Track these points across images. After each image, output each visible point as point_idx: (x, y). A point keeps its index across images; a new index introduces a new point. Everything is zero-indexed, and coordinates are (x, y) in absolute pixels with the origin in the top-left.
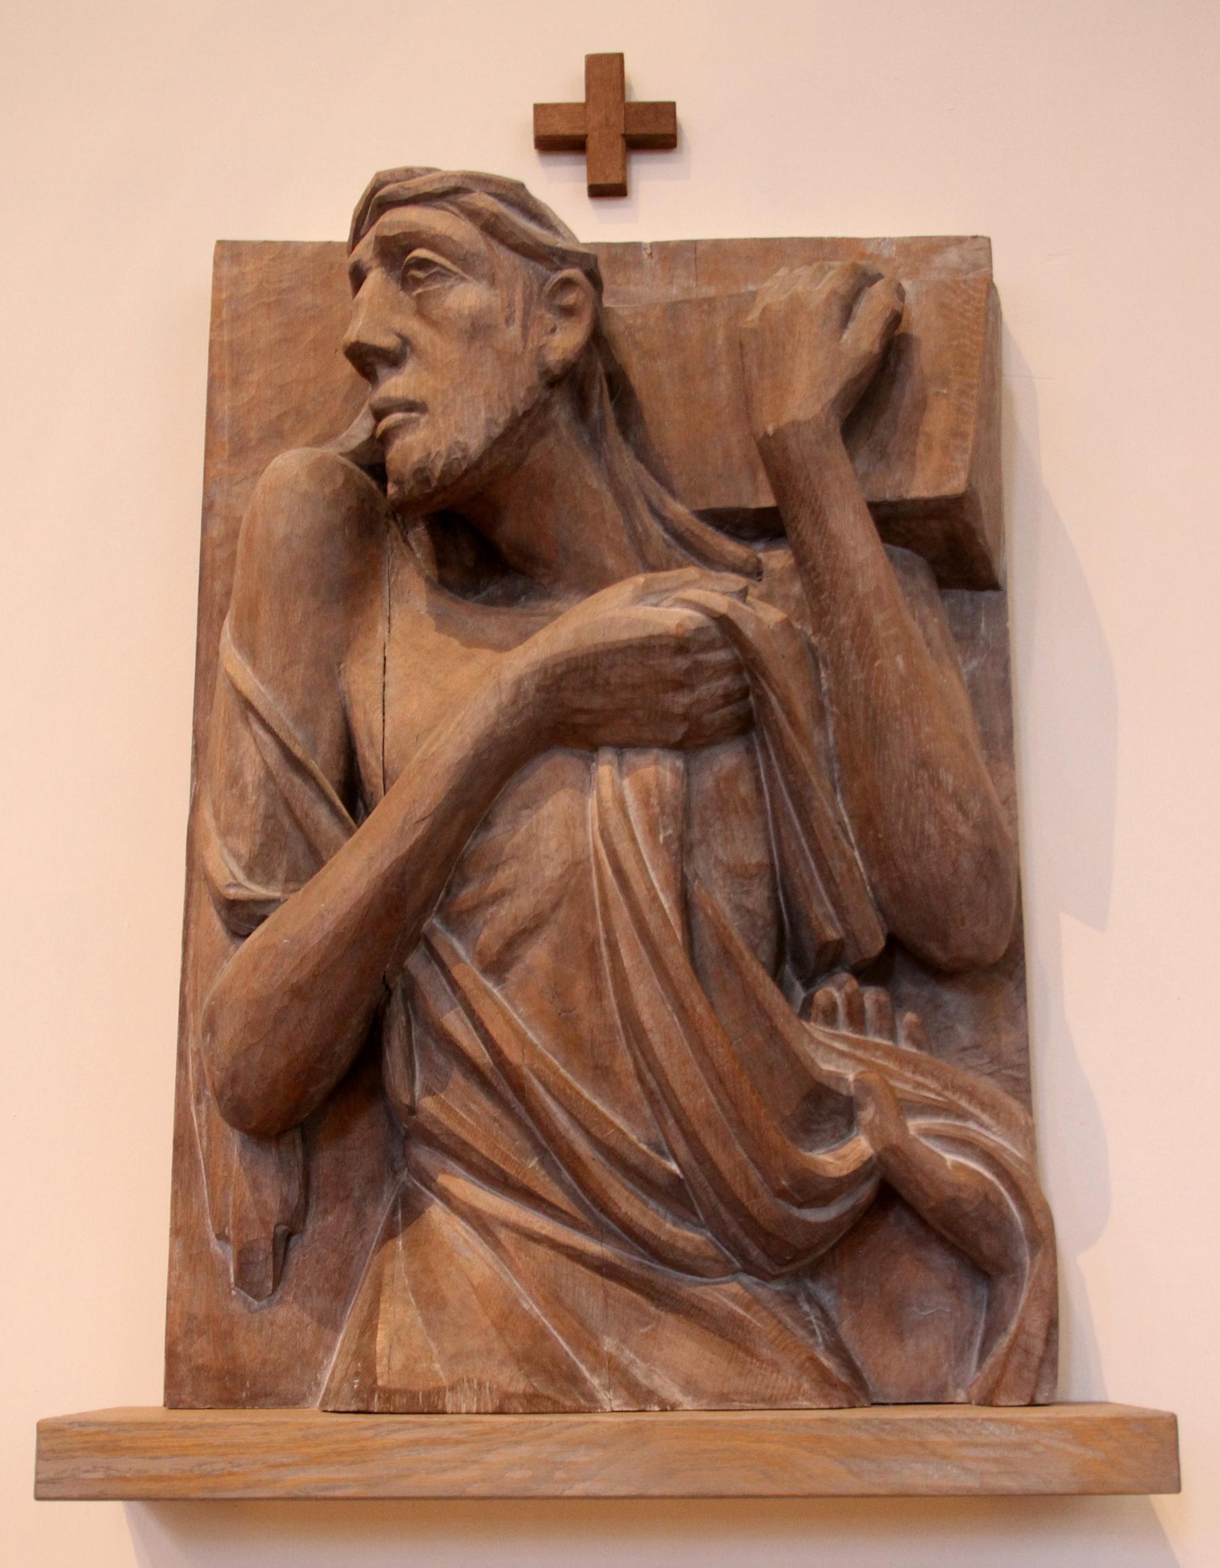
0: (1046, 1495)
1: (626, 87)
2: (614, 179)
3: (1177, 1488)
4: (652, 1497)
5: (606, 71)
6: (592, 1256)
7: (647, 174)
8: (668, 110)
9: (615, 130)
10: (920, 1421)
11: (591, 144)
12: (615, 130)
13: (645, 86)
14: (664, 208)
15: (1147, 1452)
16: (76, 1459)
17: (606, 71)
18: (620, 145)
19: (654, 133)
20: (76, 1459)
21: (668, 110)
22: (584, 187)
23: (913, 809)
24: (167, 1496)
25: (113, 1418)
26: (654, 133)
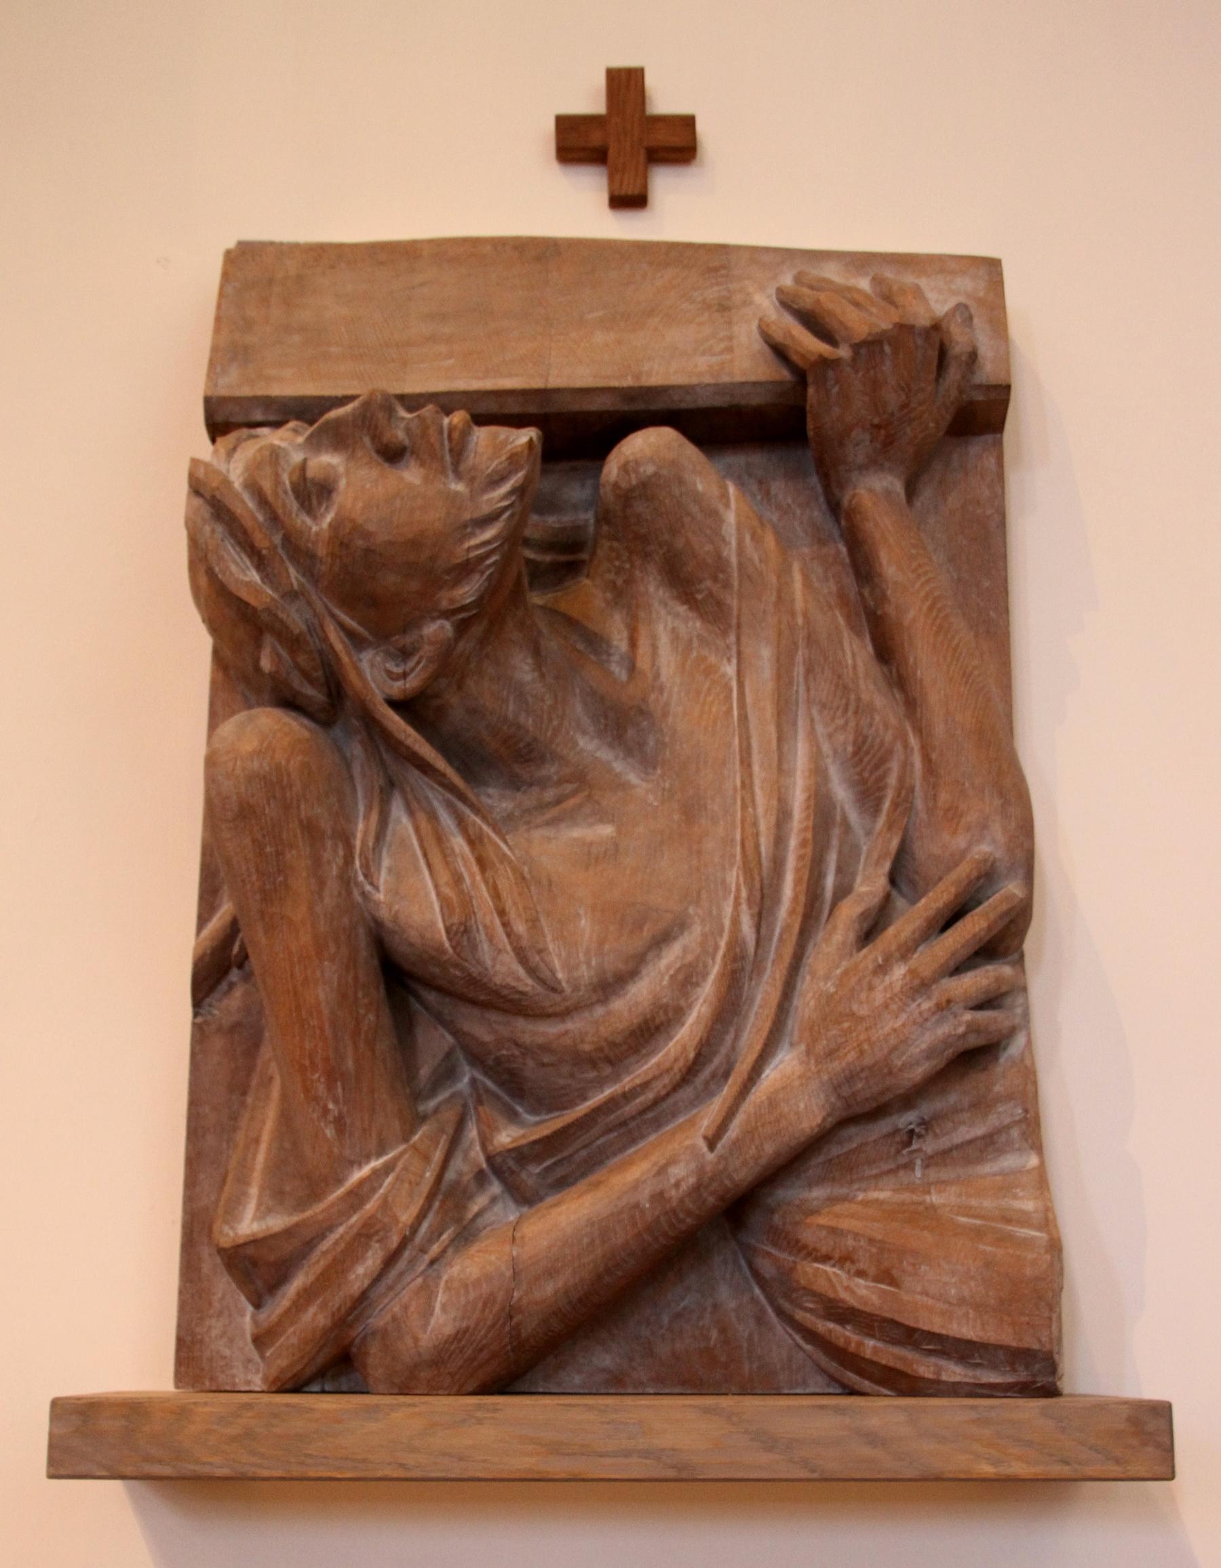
0: (1024, 1480)
1: (647, 101)
2: (630, 189)
3: (1171, 1476)
4: (432, 1480)
5: (625, 85)
6: (319, 1243)
7: (665, 185)
8: (688, 122)
9: (626, 139)
10: (287, 1405)
11: (612, 153)
12: (626, 139)
13: (664, 99)
14: (682, 210)
15: (1143, 1440)
16: (89, 1438)
17: (625, 85)
18: (642, 157)
19: (676, 144)
20: (89, 1438)
21: (688, 122)
22: (604, 197)
23: (288, 794)
24: (563, 1476)
25: (107, 1399)
26: (676, 144)
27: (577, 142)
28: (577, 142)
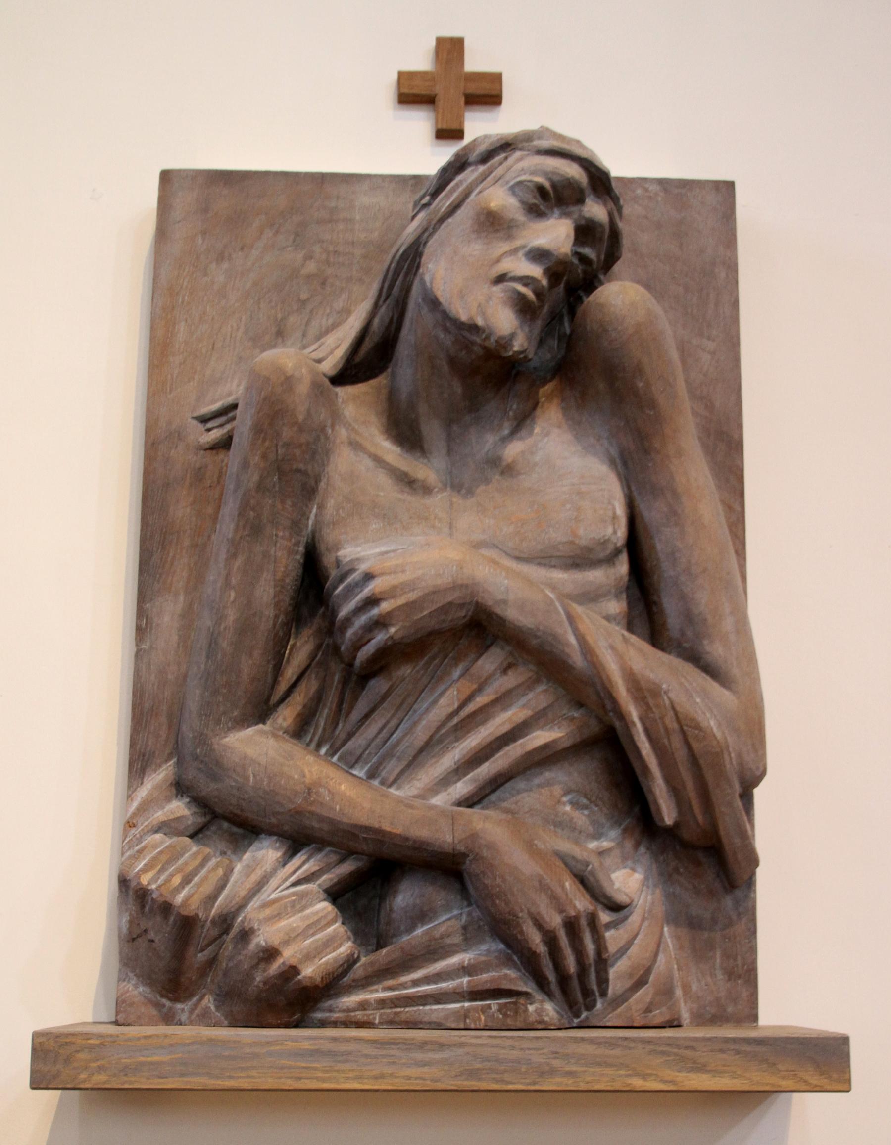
5: (450, 49)
8: (497, 78)
12: (448, 88)
13: (474, 63)
15: (823, 1060)
17: (450, 49)
19: (486, 94)
20: (54, 1060)
21: (497, 78)
26: (486, 94)
27: (412, 94)
28: (412, 94)
